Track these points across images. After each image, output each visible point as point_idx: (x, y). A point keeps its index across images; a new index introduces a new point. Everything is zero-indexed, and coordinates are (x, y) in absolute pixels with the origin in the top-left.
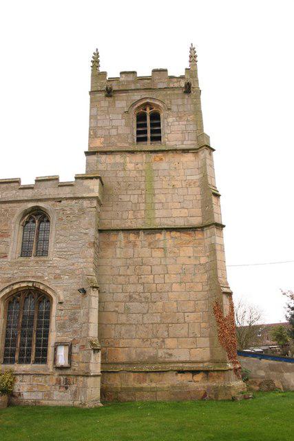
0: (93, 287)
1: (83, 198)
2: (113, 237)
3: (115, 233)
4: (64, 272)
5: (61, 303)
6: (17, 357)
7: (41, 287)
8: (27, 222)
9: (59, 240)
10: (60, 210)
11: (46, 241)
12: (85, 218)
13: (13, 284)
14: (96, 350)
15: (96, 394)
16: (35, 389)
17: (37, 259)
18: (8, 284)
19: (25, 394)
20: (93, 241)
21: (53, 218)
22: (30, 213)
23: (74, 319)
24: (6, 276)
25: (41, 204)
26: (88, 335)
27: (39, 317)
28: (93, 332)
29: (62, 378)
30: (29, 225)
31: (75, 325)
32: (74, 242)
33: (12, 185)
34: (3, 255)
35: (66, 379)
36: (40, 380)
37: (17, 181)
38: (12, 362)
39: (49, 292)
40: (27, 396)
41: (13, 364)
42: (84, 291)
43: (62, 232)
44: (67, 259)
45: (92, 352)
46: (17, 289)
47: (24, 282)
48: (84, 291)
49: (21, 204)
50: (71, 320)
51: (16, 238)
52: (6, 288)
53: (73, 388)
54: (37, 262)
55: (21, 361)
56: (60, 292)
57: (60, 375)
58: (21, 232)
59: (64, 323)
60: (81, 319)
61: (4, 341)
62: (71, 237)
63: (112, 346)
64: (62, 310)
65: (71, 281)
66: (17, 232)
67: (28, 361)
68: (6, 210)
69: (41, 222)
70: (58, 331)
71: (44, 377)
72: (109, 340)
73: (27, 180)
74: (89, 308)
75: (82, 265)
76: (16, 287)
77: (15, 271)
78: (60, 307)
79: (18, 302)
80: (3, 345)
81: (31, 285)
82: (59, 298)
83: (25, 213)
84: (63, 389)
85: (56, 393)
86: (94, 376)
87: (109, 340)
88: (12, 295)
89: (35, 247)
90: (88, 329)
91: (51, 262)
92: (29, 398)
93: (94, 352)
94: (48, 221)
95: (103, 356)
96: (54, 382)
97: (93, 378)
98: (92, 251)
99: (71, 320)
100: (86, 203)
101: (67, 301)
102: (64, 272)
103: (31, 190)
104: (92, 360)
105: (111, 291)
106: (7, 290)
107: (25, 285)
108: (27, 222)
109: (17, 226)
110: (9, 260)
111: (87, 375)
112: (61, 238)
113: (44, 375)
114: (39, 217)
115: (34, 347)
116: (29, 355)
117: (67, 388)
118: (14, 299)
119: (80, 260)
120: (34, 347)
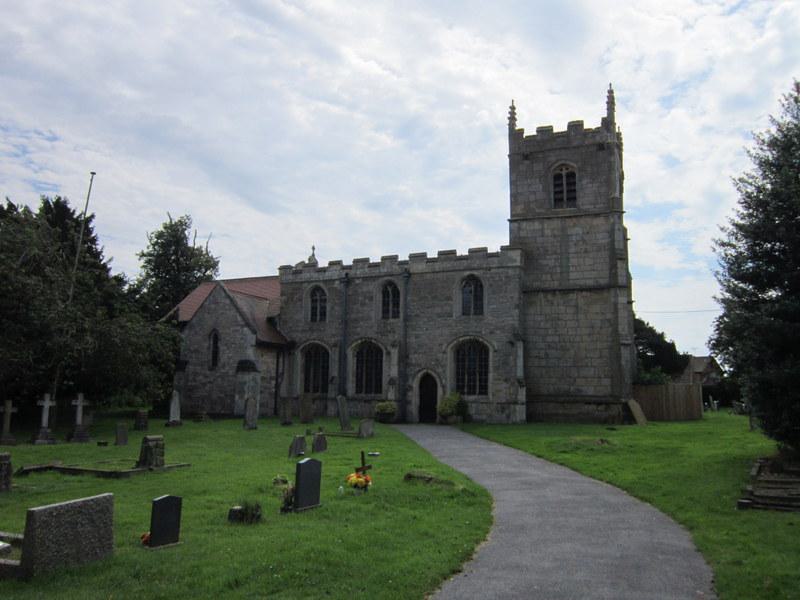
1: (508, 267)
4: (497, 328)
14: (522, 386)
15: (524, 417)
23: (506, 363)
25: (475, 273)
28: (520, 373)
39: (485, 342)
48: (512, 344)
53: (507, 411)
55: (469, 393)
56: (495, 343)
60: (512, 364)
76: (461, 339)
82: (494, 347)
83: (463, 280)
95: (529, 391)
100: (511, 272)
107: (468, 338)
111: (516, 403)
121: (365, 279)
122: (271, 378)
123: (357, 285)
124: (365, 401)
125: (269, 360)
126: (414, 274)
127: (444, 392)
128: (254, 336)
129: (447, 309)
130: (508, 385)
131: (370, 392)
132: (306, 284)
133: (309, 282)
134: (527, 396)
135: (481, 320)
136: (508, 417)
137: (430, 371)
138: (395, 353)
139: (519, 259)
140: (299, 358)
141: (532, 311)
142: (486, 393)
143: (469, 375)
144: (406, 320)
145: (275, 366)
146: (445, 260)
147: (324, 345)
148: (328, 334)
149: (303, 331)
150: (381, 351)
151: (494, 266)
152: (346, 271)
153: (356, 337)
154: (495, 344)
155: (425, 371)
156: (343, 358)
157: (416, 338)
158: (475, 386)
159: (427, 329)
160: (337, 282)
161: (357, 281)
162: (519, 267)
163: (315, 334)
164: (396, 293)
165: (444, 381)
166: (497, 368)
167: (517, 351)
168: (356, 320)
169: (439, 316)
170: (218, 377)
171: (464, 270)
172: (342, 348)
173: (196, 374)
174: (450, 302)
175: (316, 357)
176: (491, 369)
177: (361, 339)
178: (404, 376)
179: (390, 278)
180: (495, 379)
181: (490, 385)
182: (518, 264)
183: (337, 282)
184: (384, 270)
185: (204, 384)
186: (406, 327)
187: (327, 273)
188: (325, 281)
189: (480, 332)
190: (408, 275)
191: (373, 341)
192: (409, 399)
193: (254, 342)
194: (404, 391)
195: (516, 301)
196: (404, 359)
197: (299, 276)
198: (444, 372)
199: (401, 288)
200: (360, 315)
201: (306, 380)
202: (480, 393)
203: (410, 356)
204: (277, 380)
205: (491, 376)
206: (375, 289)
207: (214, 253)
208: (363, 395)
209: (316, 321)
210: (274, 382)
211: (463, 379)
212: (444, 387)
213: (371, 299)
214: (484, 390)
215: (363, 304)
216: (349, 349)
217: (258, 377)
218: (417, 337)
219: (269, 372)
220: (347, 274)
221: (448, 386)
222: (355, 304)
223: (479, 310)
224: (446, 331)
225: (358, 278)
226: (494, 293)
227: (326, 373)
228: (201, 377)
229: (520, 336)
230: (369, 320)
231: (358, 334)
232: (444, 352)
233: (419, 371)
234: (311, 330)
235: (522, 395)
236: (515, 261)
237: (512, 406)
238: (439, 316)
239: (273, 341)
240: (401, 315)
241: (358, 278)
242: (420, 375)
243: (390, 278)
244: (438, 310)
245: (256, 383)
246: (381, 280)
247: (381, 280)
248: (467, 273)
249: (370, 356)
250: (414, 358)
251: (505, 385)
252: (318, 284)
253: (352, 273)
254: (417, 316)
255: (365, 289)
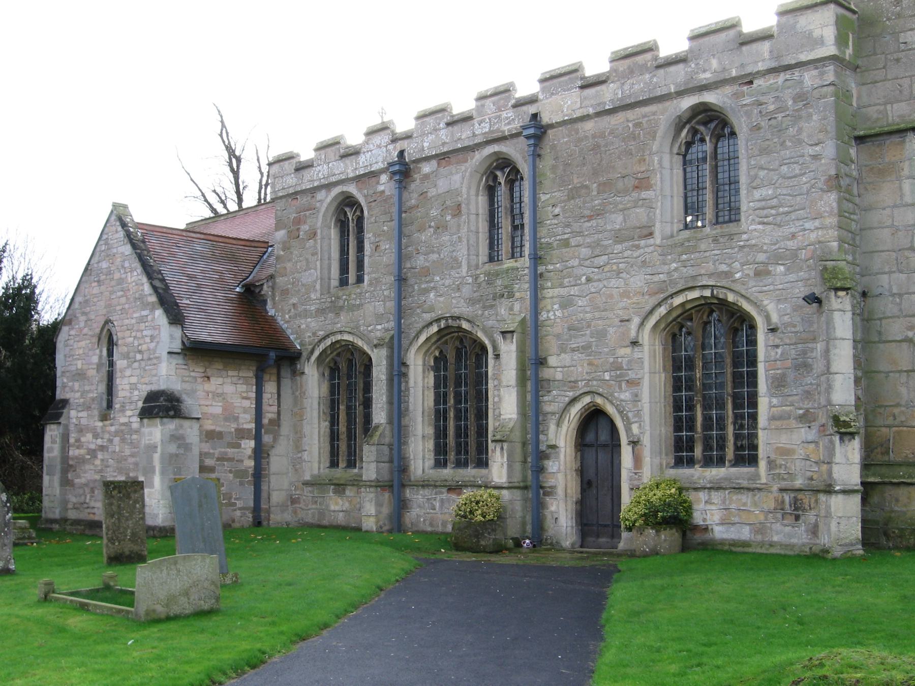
0: (837, 289)
1: (800, 65)
2: (890, 152)
3: (896, 139)
4: (777, 258)
5: (773, 330)
6: (698, 452)
7: (731, 298)
8: (689, 145)
9: (758, 182)
10: (753, 104)
11: (734, 182)
12: (810, 116)
13: (672, 296)
14: (846, 435)
15: (854, 530)
16: (736, 519)
17: (718, 230)
18: (662, 296)
19: (717, 529)
20: (833, 172)
21: (741, 124)
22: (689, 121)
23: (803, 366)
24: (656, 278)
25: (710, 98)
26: (829, 403)
27: (736, 364)
28: (843, 393)
29: (787, 498)
30: (694, 149)
31: (809, 380)
32: (794, 182)
33: (639, 59)
34: (645, 232)
35: (796, 499)
36: (744, 501)
37: (649, 49)
38: (691, 462)
39: (746, 306)
40: (719, 533)
41: (693, 467)
42: (814, 299)
43: (763, 160)
44: (780, 226)
45: (837, 438)
46: (683, 305)
47: (692, 288)
48: (814, 299)
49: (667, 104)
50: (797, 367)
51: (667, 192)
52: (659, 305)
53: (811, 517)
54: (715, 240)
55: (708, 462)
56: (771, 305)
57: (782, 490)
58: (678, 172)
59: (784, 375)
60: (819, 366)
61: (671, 421)
62: (784, 169)
63: (902, 424)
64: (777, 346)
65: (792, 277)
66: (667, 173)
67: (721, 462)
68: (638, 125)
69: (718, 137)
70: (772, 395)
71: (750, 493)
72: (896, 411)
73: (673, 44)
74: (830, 340)
75: (813, 236)
76: (678, 301)
77: (674, 265)
78: (773, 339)
79: (689, 333)
80: (671, 429)
81: (707, 293)
82: (768, 318)
83: (680, 124)
84: (790, 520)
85: (778, 526)
86: (844, 492)
87: (896, 411)
88: (674, 320)
89: (712, 195)
90: (829, 388)
91: (744, 237)
92: (725, 536)
93: (841, 439)
94: (733, 134)
95: (868, 449)
96: (772, 505)
97: (840, 496)
98: (832, 198)
99: (797, 367)
100: (809, 78)
101: (786, 325)
102: (777, 258)
103: (681, 66)
104: (838, 457)
105: (895, 291)
106: (663, 310)
107: (695, 294)
108: (689, 145)
109: (666, 158)
110: (658, 241)
111: (829, 490)
112: (762, 173)
113: (749, 489)
114: (712, 125)
115: (730, 430)
116: (722, 447)
117: (797, 518)
118: (682, 327)
119: (808, 225)
120: (730, 430)
121: (443, 157)
122: (241, 433)
123: (426, 177)
124: (451, 489)
125: (229, 389)
126: (551, 126)
127: (637, 460)
128: (177, 332)
129: (639, 215)
130: (812, 435)
131: (466, 465)
132: (321, 195)
133: (329, 186)
134: (866, 466)
135: (731, 236)
136: (814, 531)
137: (599, 400)
138: (509, 351)
139: (830, 33)
140: (313, 382)
141: (885, 194)
142: (753, 460)
143: (706, 407)
144: (536, 259)
145: (250, 404)
146: (631, 72)
147: (360, 343)
148: (367, 319)
149: (321, 312)
150: (484, 349)
151: (761, 67)
152: (400, 146)
153: (428, 317)
154: (771, 307)
155: (587, 400)
156: (398, 372)
157: (563, 307)
158: (722, 440)
159: (589, 280)
160: (384, 178)
161: (426, 168)
162: (833, 58)
163: (343, 317)
164: (514, 176)
165: (635, 429)
166: (778, 383)
167: (830, 324)
168: (426, 272)
169: (619, 237)
170: (116, 433)
171: (680, 94)
172: (396, 346)
173: (81, 430)
174: (644, 194)
175: (347, 369)
176: (762, 386)
177: (438, 320)
178: (533, 414)
179: (495, 148)
180: (773, 418)
181: (763, 438)
182: (830, 49)
183: (384, 178)
184: (481, 129)
185: (93, 453)
186: (537, 278)
187: (362, 159)
188: (358, 179)
189: (728, 274)
190: (538, 131)
191: (465, 325)
192: (551, 482)
193: (177, 346)
194: (536, 457)
195: (827, 164)
196: (533, 365)
197: (307, 174)
198: (636, 398)
199: (525, 168)
200: (434, 257)
201: (440, 434)
202: (739, 461)
203: (552, 361)
204: (258, 438)
205: (763, 403)
206: (462, 181)
207: (295, 151)
208: (447, 472)
209: (347, 284)
210: (249, 445)
211: (691, 420)
212: (634, 443)
213: (457, 211)
214: (747, 455)
215: (441, 227)
216: (413, 350)
217: (191, 431)
218: (566, 303)
219: (229, 416)
220: (402, 153)
221: (646, 440)
222: (421, 230)
223: (728, 213)
224: (638, 281)
225: (427, 159)
226: (765, 151)
227: (368, 418)
228: (89, 436)
229: (843, 279)
230: (455, 277)
231: (431, 309)
232: (635, 343)
233: (574, 401)
234: (336, 309)
235: (848, 464)
236: (821, 42)
237: (822, 497)
238: (619, 237)
239: (251, 343)
240: (527, 250)
241: (427, 159)
242: (575, 410)
243: (495, 148)
244: (616, 221)
245: (187, 447)
246: (479, 156)
247: (479, 156)
248: (688, 102)
249: (461, 359)
250: (558, 364)
251: (804, 433)
252: (345, 188)
253: (412, 150)
254: (566, 243)
255: (442, 185)
